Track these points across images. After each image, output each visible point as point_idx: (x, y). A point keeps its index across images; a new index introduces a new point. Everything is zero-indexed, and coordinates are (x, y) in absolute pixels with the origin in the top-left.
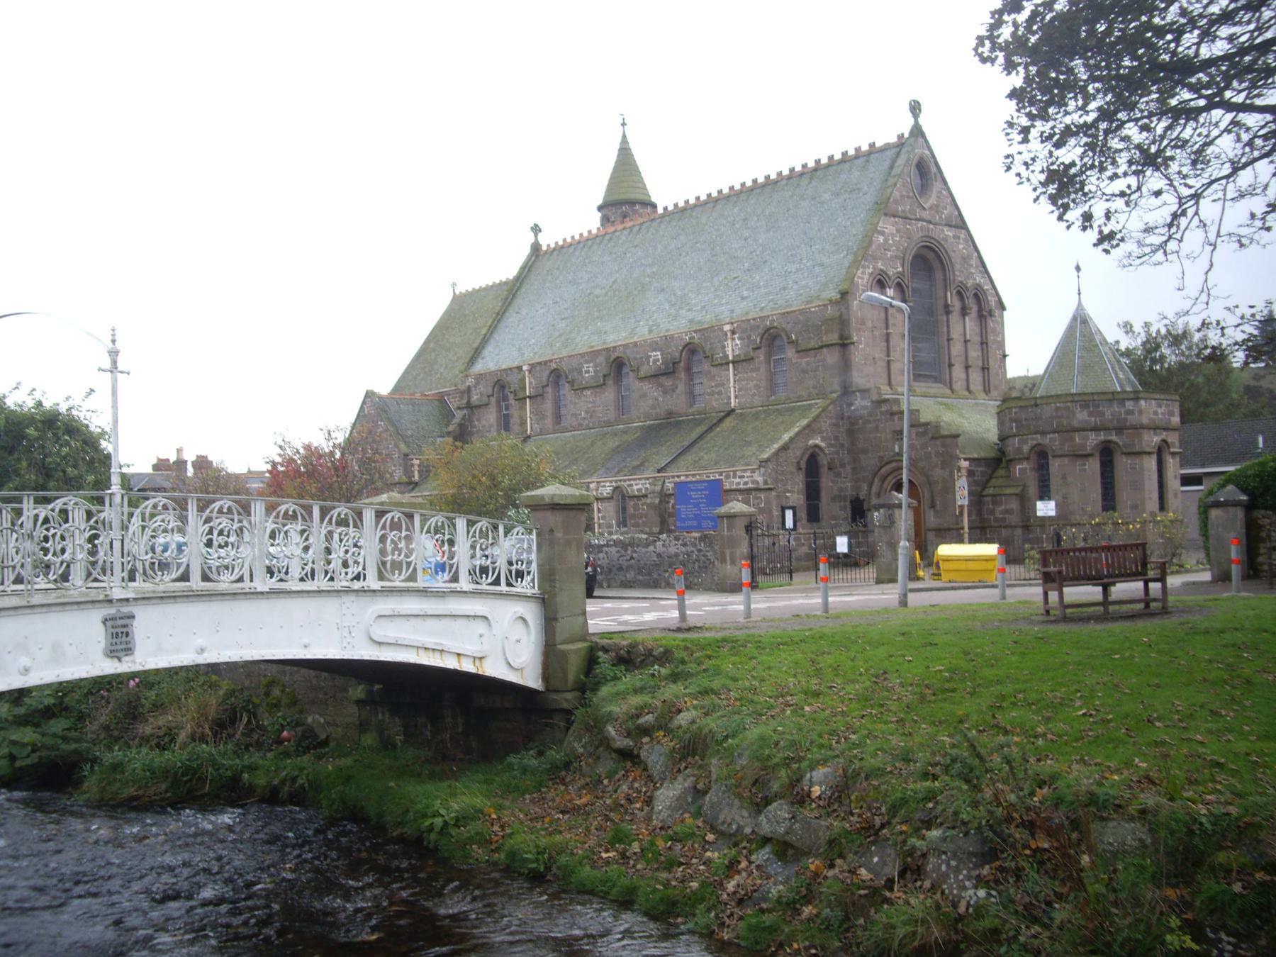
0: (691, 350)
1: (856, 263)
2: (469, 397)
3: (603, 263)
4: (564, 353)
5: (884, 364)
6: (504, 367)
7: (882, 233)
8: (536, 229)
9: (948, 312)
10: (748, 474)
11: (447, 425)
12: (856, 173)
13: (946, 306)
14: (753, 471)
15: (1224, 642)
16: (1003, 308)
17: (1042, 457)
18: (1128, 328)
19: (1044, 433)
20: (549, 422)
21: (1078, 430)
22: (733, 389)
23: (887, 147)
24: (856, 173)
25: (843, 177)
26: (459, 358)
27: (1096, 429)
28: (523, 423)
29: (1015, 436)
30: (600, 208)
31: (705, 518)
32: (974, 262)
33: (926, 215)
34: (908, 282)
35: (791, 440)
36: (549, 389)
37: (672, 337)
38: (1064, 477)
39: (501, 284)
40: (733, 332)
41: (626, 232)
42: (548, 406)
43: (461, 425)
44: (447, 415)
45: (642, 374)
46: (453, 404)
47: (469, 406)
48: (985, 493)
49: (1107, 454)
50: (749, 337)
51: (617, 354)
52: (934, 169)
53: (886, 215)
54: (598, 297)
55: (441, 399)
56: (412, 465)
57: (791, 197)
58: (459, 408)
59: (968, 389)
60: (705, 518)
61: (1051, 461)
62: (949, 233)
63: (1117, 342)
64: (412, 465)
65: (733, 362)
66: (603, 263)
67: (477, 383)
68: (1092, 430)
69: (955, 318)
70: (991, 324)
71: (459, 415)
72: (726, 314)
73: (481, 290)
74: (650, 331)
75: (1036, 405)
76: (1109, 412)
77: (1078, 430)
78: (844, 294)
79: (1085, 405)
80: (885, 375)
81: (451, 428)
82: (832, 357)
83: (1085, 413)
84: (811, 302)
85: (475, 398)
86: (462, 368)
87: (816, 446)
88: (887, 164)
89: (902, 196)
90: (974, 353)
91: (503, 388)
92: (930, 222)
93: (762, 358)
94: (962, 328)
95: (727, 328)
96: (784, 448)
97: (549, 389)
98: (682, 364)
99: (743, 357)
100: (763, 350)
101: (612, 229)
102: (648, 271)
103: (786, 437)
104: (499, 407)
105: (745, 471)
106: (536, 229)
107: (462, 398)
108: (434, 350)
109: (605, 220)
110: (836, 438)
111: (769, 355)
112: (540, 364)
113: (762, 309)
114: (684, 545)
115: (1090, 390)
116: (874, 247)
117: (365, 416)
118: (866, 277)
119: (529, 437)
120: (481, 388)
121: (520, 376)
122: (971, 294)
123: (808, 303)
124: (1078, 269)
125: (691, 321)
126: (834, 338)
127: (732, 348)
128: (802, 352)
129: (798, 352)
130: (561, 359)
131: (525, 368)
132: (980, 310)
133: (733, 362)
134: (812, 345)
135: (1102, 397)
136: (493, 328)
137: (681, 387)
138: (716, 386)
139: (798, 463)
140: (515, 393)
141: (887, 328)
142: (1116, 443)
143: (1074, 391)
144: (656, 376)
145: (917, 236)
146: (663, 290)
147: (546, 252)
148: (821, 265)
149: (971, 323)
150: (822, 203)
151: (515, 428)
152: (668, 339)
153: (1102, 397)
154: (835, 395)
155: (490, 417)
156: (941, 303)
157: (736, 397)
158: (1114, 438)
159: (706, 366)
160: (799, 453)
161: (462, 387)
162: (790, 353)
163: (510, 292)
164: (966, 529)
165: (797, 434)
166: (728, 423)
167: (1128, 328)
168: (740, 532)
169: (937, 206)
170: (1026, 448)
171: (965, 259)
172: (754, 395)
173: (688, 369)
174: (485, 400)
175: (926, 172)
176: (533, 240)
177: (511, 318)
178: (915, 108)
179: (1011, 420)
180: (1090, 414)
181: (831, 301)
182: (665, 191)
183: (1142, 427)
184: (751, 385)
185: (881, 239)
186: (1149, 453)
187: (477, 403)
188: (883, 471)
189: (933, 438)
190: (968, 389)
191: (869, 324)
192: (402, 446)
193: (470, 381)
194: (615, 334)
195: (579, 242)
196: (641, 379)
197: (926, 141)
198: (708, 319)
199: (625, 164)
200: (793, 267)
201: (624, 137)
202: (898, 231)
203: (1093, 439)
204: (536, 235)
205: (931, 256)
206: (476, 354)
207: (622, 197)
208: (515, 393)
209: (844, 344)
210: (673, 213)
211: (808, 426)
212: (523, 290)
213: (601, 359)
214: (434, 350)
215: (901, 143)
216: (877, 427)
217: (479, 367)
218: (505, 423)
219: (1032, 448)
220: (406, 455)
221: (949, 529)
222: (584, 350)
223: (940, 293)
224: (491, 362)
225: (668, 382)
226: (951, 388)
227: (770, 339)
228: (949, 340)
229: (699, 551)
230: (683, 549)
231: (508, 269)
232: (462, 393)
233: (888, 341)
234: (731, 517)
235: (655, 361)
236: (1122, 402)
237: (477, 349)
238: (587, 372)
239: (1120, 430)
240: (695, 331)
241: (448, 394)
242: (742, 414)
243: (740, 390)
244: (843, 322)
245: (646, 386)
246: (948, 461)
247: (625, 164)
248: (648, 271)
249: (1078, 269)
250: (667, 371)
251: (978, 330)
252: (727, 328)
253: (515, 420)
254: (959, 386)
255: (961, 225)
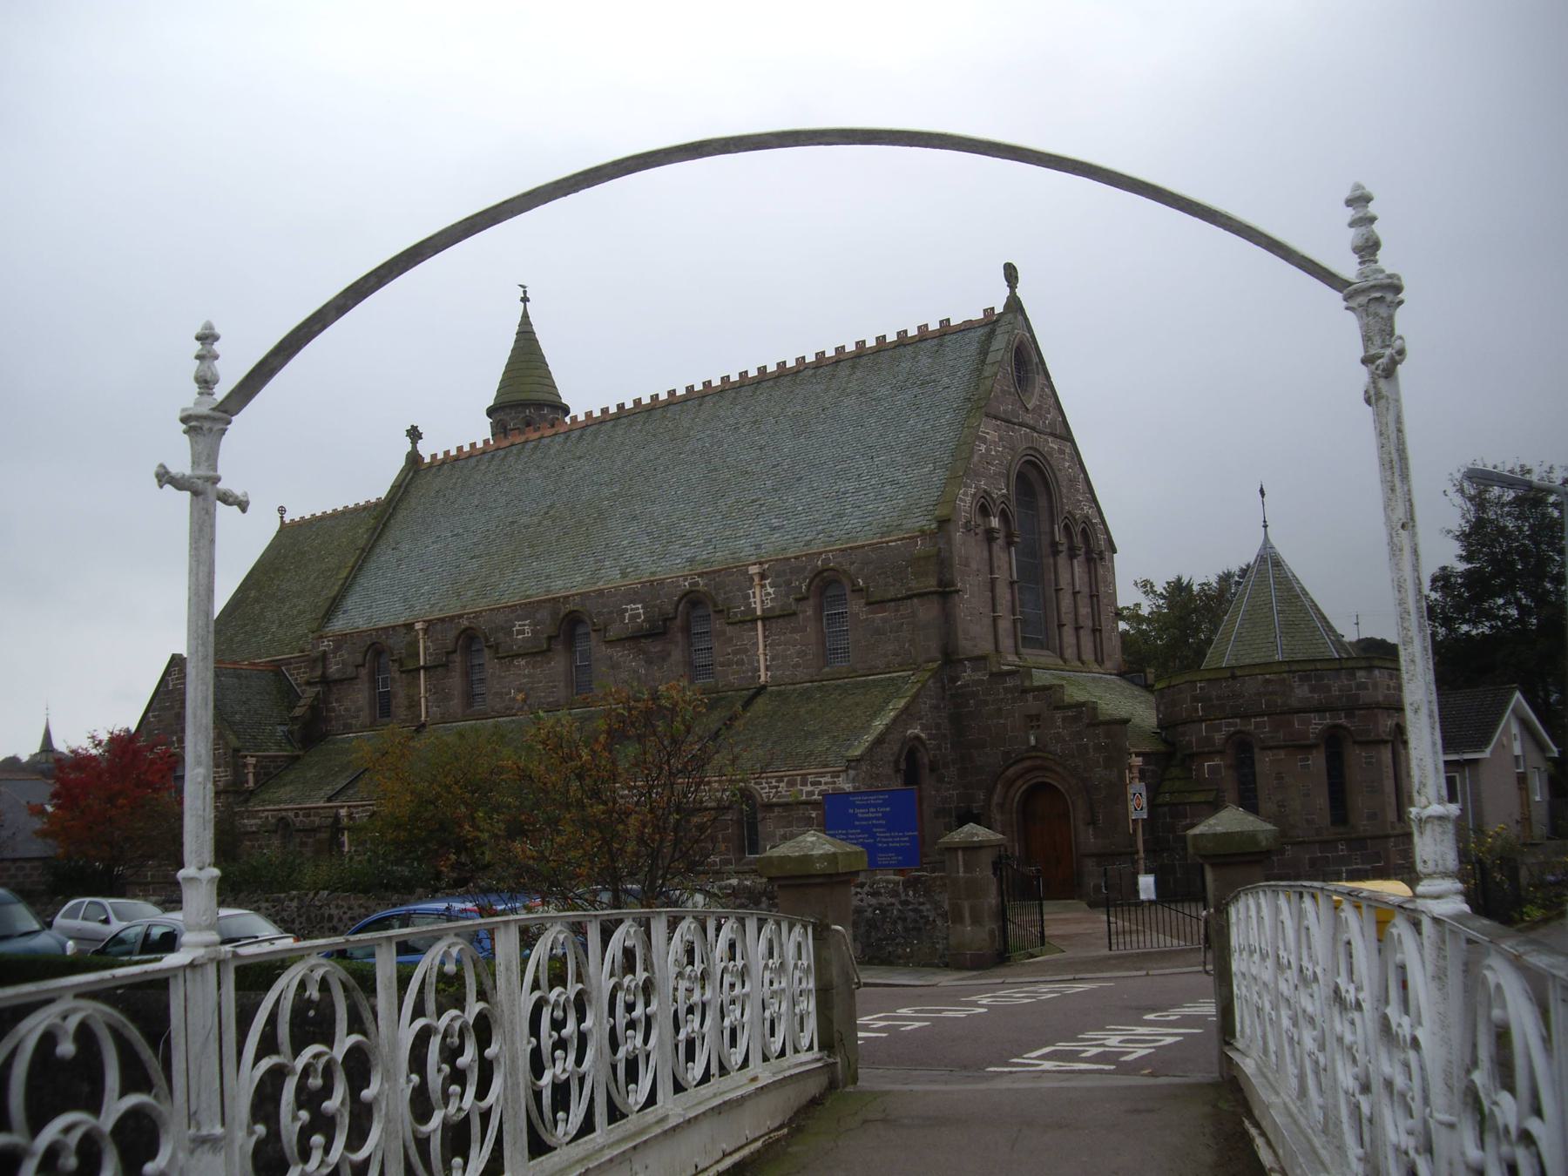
0: (693, 600)
1: (955, 479)
2: (325, 667)
3: (528, 480)
4: (483, 604)
5: (987, 621)
6: (382, 624)
7: (984, 441)
8: (414, 434)
9: (1056, 553)
10: (827, 779)
11: (291, 707)
12: (925, 361)
13: (1054, 544)
14: (836, 775)
15: (1343, 988)
16: (1114, 551)
17: (1243, 750)
18: (1147, 587)
19: (1246, 717)
20: (456, 704)
21: (1298, 711)
22: (762, 658)
23: (968, 326)
24: (925, 361)
25: (905, 365)
26: (301, 612)
27: (1320, 710)
28: (413, 705)
29: (1201, 720)
30: (491, 412)
31: (883, 850)
32: (1081, 486)
33: (1029, 419)
34: (1013, 508)
35: (888, 728)
36: (457, 658)
37: (661, 582)
38: (1279, 777)
39: (358, 510)
40: (763, 576)
41: (560, 439)
42: (455, 682)
43: (312, 708)
44: (289, 695)
45: (611, 635)
46: (298, 677)
47: (325, 681)
48: (1160, 800)
49: (1334, 742)
50: (788, 583)
51: (570, 607)
52: (1036, 359)
53: (987, 415)
54: (527, 527)
55: (276, 669)
56: (245, 765)
57: (826, 391)
58: (309, 683)
59: (1079, 658)
60: (883, 850)
61: (1258, 754)
62: (1054, 445)
63: (1138, 605)
64: (245, 765)
65: (764, 619)
66: (528, 480)
67: (338, 648)
68: (1317, 710)
69: (1062, 559)
70: (1101, 571)
71: (311, 692)
72: (748, 550)
73: (324, 517)
74: (624, 575)
75: (1234, 677)
76: (1336, 686)
77: (1298, 711)
78: (943, 522)
79: (1305, 678)
80: (991, 638)
81: (298, 712)
82: (927, 612)
83: (1306, 688)
84: (889, 533)
85: (333, 669)
86: (315, 625)
87: (917, 738)
88: (973, 349)
89: (1003, 391)
90: (1084, 610)
91: (378, 650)
92: (1033, 429)
93: (810, 612)
94: (1071, 574)
95: (753, 570)
96: (879, 741)
97: (457, 658)
98: (678, 622)
99: (777, 613)
100: (811, 601)
101: (536, 435)
102: (606, 492)
103: (879, 724)
104: (373, 681)
105: (823, 775)
106: (414, 434)
107: (312, 670)
108: (257, 600)
109: (499, 429)
110: (938, 726)
111: (819, 609)
112: (442, 620)
113: (807, 544)
114: (875, 894)
115: (1299, 657)
116: (976, 458)
117: (169, 692)
118: (968, 499)
119: (424, 725)
120: (344, 654)
121: (408, 638)
122: (1079, 529)
123: (883, 535)
124: (1262, 492)
125: (691, 560)
126: (931, 583)
127: (760, 598)
128: (875, 604)
129: (868, 604)
130: (478, 614)
131: (418, 626)
132: (1089, 552)
133: (764, 619)
134: (891, 594)
135: (1326, 665)
136: (357, 569)
137: (677, 655)
138: (735, 653)
139: (897, 762)
140: (400, 662)
141: (992, 572)
142: (1345, 728)
143: (1278, 657)
144: (635, 638)
145: (1022, 447)
146: (635, 518)
147: (431, 465)
148: (893, 483)
149: (1079, 567)
150: (878, 400)
151: (402, 713)
152: (654, 586)
153: (1326, 665)
154: (935, 665)
155: (359, 698)
156: (1045, 540)
157: (767, 668)
158: (1343, 721)
159: (718, 624)
160: (896, 748)
161: (314, 654)
162: (856, 606)
163: (374, 525)
164: (1142, 854)
165: (895, 720)
166: (760, 704)
167: (1147, 587)
168: (985, 873)
169: (1040, 407)
170: (1219, 737)
171: (1072, 480)
172: (797, 666)
173: (687, 630)
174: (350, 671)
175: (1026, 361)
176: (409, 448)
177: (385, 555)
178: (1011, 273)
179: (1195, 699)
180: (1313, 689)
181: (923, 532)
182: (585, 388)
183: (1378, 706)
184: (792, 650)
185: (983, 447)
186: (1386, 742)
187: (337, 676)
188: (1012, 771)
189: (1090, 725)
190: (1079, 658)
191: (974, 566)
192: (231, 737)
193: (326, 645)
194: (566, 579)
195: (484, 452)
196: (610, 643)
197: (1026, 320)
198: (721, 557)
199: (526, 352)
200: (851, 486)
201: (525, 316)
202: (1001, 439)
203: (1316, 725)
204: (414, 443)
205: (1033, 475)
206: (334, 606)
207: (523, 396)
208: (400, 662)
209: (946, 592)
210: (631, 413)
211: (906, 708)
212: (399, 517)
213: (544, 614)
214: (257, 600)
215: (991, 322)
216: (1000, 709)
217: (339, 624)
218: (383, 707)
219: (1230, 737)
220: (236, 750)
221: (1120, 854)
222: (516, 600)
223: (1045, 527)
224: (357, 616)
225: (655, 648)
226: (1062, 656)
227: (823, 586)
228: (1057, 591)
229: (905, 903)
230: (873, 901)
231: (376, 487)
232: (315, 660)
233: (993, 590)
234: (972, 849)
235: (634, 617)
236: (1352, 672)
237: (334, 599)
238: (519, 632)
239: (1350, 712)
240: (699, 575)
241: (288, 662)
242: (780, 693)
243: (773, 659)
244: (942, 563)
245: (617, 653)
246: (1115, 758)
247: (526, 352)
248: (606, 492)
249: (1262, 492)
250: (655, 631)
251: (1086, 579)
252: (753, 570)
253: (400, 700)
254: (1070, 652)
255: (1067, 437)
